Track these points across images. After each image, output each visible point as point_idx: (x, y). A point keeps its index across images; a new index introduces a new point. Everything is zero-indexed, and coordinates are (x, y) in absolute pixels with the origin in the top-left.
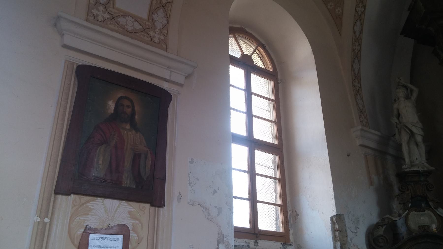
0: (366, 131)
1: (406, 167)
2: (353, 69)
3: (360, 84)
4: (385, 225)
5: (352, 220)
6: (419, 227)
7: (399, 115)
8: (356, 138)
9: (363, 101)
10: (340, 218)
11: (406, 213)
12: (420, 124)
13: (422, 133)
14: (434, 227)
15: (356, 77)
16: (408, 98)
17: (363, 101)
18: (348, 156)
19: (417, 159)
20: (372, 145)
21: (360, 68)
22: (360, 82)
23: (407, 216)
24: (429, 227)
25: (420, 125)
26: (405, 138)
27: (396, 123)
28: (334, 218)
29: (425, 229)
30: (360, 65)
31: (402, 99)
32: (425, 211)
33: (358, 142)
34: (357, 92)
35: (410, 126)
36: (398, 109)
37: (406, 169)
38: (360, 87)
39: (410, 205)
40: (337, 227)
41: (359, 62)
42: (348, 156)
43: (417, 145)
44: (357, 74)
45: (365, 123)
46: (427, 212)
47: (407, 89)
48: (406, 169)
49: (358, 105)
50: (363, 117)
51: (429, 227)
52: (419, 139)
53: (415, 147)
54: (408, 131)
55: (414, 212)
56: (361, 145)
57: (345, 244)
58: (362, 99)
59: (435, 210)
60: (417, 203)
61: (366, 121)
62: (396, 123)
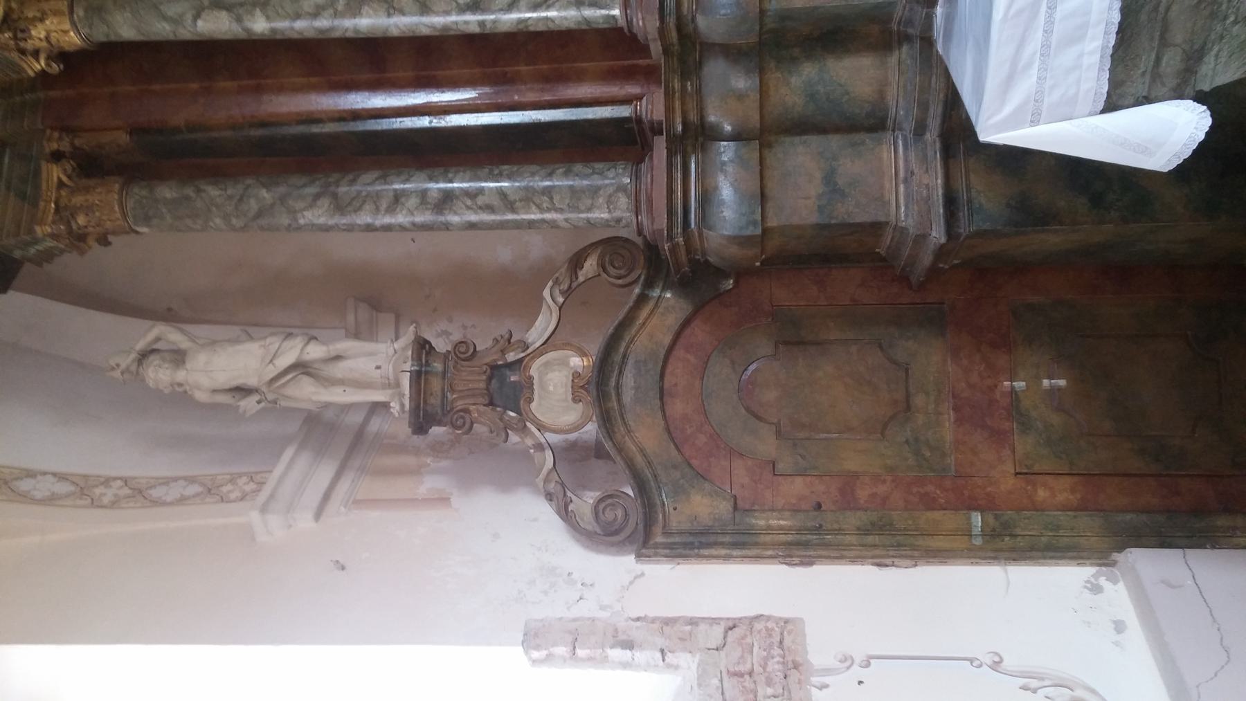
0: (272, 496)
1: (398, 408)
2: (51, 500)
3: (115, 479)
4: (565, 495)
5: (546, 593)
6: (574, 400)
7: (242, 391)
8: (290, 526)
9: (176, 479)
10: (536, 635)
11: (533, 429)
12: (268, 340)
13: (298, 343)
14: (576, 361)
15: (84, 491)
16: (178, 357)
17: (176, 479)
18: (343, 568)
19: (378, 367)
20: (325, 473)
21: (54, 474)
22: (107, 481)
23: (541, 427)
24: (576, 375)
25: (274, 342)
26: (307, 392)
27: (259, 402)
28: (536, 654)
29: (579, 386)
30: (45, 473)
31: (181, 375)
32: (531, 378)
33: (305, 521)
34: (139, 493)
35: (271, 372)
36: (215, 391)
37: (402, 405)
38: (126, 481)
39: (512, 414)
40: (561, 650)
41: (31, 474)
42: (343, 568)
43: (338, 358)
44: (72, 488)
45: (252, 486)
46: (534, 371)
47: (153, 351)
48: (402, 405)
49: (182, 500)
50: (229, 487)
51: (576, 375)
52: (315, 352)
53: (343, 365)
54: (290, 376)
55: (533, 405)
56: (318, 515)
57: (616, 630)
58: (167, 481)
59: (529, 351)
60: (506, 388)
61: (244, 479)
62: (259, 402)
